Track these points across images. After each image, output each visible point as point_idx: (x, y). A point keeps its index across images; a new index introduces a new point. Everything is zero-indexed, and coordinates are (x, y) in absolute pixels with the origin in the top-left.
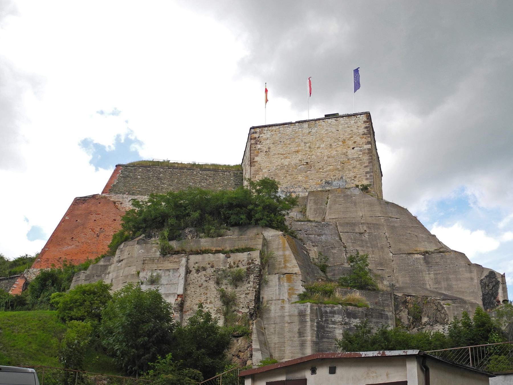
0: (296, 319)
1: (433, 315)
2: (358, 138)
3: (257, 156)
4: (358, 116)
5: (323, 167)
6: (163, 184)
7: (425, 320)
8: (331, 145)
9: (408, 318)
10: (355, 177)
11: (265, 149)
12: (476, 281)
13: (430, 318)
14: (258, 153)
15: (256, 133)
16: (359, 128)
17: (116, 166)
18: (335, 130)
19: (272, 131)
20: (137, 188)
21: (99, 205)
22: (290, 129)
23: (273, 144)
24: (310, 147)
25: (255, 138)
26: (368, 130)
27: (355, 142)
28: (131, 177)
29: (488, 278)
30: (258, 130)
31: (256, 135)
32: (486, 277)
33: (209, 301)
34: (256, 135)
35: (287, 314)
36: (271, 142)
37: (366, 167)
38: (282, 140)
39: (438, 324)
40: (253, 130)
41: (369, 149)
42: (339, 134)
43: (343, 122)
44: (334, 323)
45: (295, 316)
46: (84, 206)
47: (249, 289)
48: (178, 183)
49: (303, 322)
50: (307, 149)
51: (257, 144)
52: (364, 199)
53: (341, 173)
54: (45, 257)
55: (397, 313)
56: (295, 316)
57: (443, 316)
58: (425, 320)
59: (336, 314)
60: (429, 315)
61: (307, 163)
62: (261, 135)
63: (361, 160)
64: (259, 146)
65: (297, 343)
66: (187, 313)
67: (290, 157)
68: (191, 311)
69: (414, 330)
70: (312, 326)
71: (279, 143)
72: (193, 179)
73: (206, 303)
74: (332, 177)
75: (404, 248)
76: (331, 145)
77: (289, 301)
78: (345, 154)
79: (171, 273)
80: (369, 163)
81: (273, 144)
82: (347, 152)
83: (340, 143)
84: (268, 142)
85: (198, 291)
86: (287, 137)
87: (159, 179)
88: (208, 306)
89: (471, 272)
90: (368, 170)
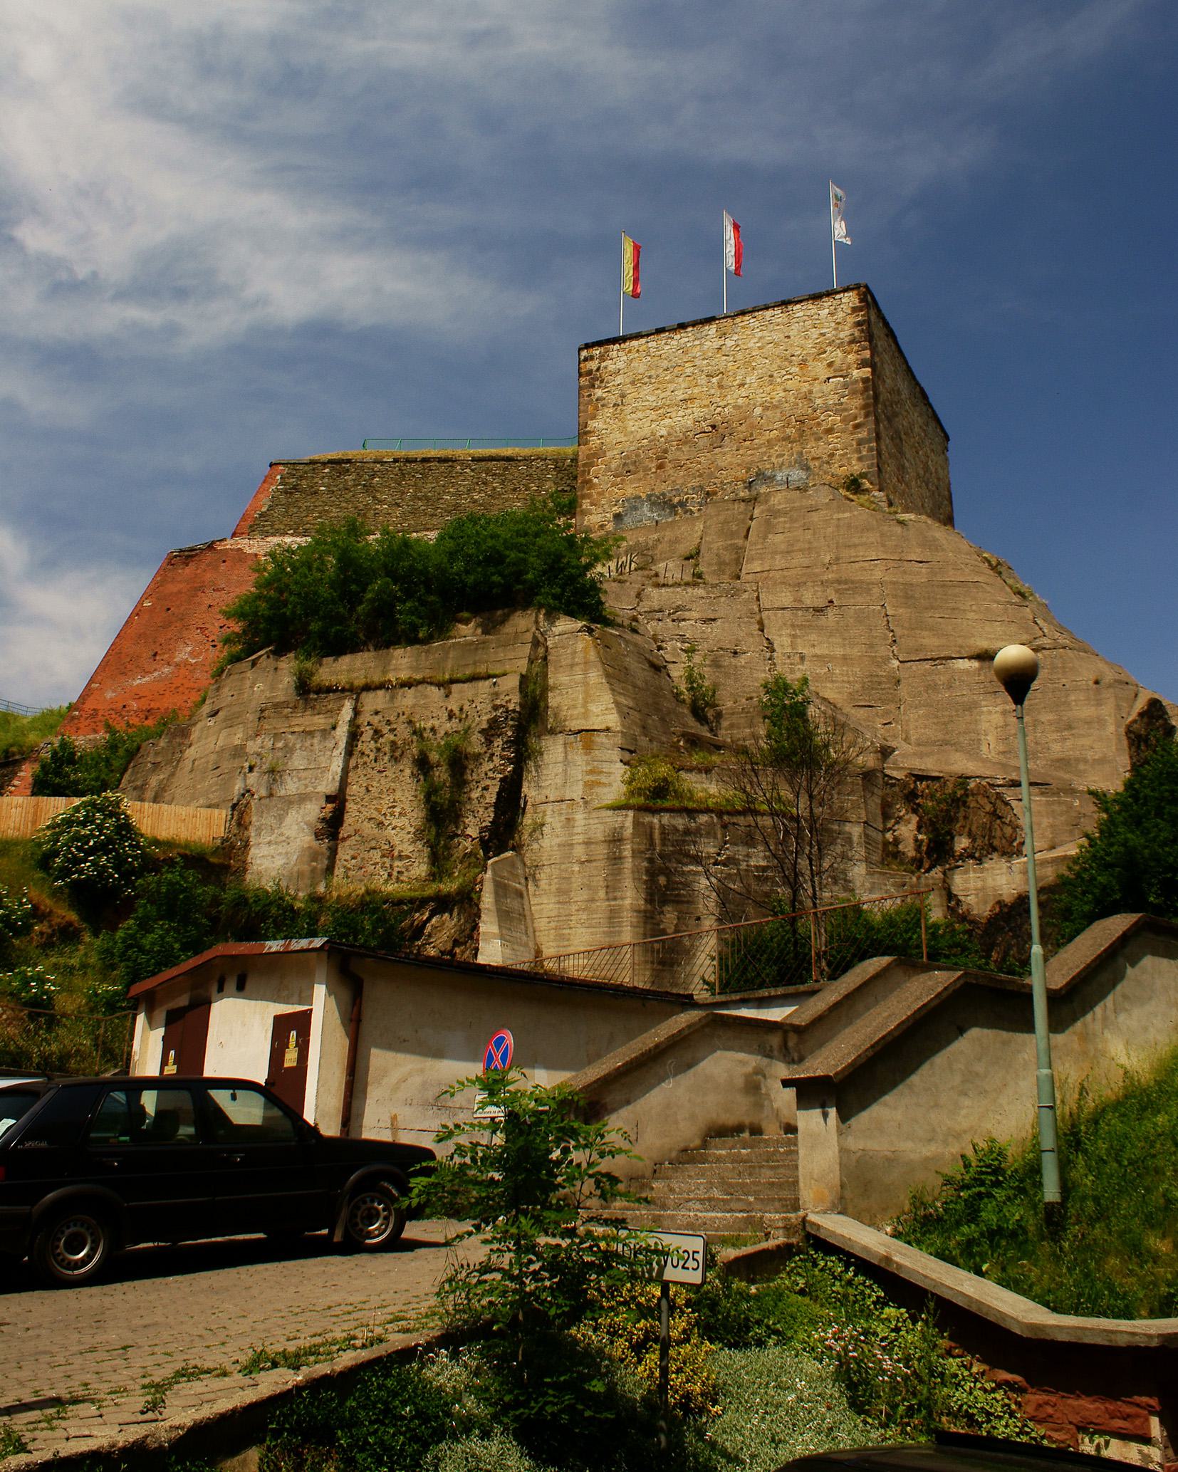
0: (602, 851)
1: (984, 828)
2: (839, 353)
3: (594, 417)
4: (838, 297)
5: (751, 435)
6: (381, 502)
7: (963, 846)
8: (771, 376)
9: (916, 840)
10: (832, 455)
11: (613, 399)
12: (1111, 728)
13: (974, 840)
14: (596, 409)
15: (591, 358)
16: (840, 327)
17: (271, 465)
18: (782, 336)
19: (630, 351)
20: (315, 518)
21: (223, 567)
22: (675, 343)
23: (633, 383)
24: (720, 386)
25: (590, 372)
26: (862, 331)
27: (830, 365)
28: (303, 491)
29: (1145, 720)
30: (596, 352)
31: (593, 365)
32: (1141, 715)
33: (397, 810)
34: (593, 365)
35: (580, 838)
36: (628, 381)
37: (857, 426)
38: (653, 373)
39: (995, 855)
40: (584, 353)
41: (865, 380)
42: (792, 345)
43: (801, 314)
44: (697, 860)
45: (596, 843)
46: (188, 570)
47: (490, 774)
48: (415, 498)
49: (615, 859)
50: (712, 391)
51: (593, 386)
52: (841, 516)
53: (797, 447)
54: (89, 705)
55: (889, 825)
56: (596, 843)
57: (1008, 830)
58: (962, 843)
59: (701, 836)
60: (974, 829)
61: (714, 427)
62: (603, 364)
63: (846, 410)
64: (599, 393)
65: (600, 916)
66: (347, 843)
67: (673, 415)
68: (357, 838)
69: (933, 873)
70: (635, 870)
71: (646, 380)
72: (453, 485)
73: (392, 814)
74: (773, 460)
75: (930, 642)
76: (771, 376)
77: (586, 803)
78: (808, 397)
79: (316, 741)
80: (867, 416)
81: (633, 383)
82: (811, 392)
83: (795, 369)
84: (619, 380)
85: (374, 784)
86: (665, 364)
87: (368, 488)
88: (394, 823)
89: (1099, 703)
90: (863, 434)
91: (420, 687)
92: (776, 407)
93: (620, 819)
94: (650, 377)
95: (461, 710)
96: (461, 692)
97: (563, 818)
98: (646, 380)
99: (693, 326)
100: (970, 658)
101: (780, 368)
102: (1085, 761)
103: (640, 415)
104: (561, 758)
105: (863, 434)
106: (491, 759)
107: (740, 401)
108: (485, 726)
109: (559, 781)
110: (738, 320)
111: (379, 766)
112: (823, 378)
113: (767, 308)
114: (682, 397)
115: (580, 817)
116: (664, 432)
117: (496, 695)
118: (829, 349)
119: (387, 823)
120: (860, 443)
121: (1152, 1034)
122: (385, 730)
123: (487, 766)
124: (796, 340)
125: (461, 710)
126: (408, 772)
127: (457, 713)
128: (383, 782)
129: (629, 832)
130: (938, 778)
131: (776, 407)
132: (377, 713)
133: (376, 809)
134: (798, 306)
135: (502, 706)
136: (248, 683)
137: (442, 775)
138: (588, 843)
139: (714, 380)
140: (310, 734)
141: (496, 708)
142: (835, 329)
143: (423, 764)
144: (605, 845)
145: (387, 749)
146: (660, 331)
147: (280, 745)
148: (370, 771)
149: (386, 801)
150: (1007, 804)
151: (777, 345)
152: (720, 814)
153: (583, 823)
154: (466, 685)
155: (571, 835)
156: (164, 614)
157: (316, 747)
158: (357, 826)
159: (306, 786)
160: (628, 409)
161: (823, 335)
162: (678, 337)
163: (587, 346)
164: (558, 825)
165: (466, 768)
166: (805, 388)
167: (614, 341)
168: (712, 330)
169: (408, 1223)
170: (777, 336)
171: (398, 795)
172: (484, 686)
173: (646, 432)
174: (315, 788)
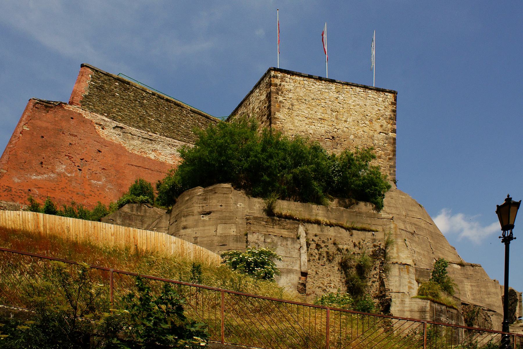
4: (386, 94)
5: (349, 147)
15: (277, 77)
19: (295, 82)
27: (382, 126)
30: (279, 75)
33: (332, 285)
34: (278, 81)
35: (408, 309)
36: (295, 98)
37: (390, 159)
40: (273, 73)
45: (415, 312)
56: (415, 312)
57: (490, 325)
62: (283, 83)
63: (386, 150)
73: (330, 287)
76: (358, 122)
78: (372, 138)
79: (289, 243)
81: (297, 100)
82: (373, 136)
84: (291, 95)
85: (320, 271)
86: (312, 96)
91: (336, 227)
92: (360, 138)
93: (424, 303)
94: (305, 100)
95: (359, 243)
96: (358, 235)
97: (400, 300)
98: (303, 101)
99: (325, 81)
100: (458, 264)
101: (362, 120)
102: (495, 306)
103: (301, 118)
104: (397, 274)
106: (375, 269)
107: (345, 129)
108: (371, 254)
109: (397, 284)
110: (345, 87)
111: (321, 262)
112: (379, 131)
113: (357, 86)
114: (320, 117)
115: (407, 300)
116: (311, 132)
117: (374, 240)
118: (381, 118)
119: (328, 290)
122: (323, 245)
123: (373, 272)
124: (369, 108)
125: (359, 243)
126: (336, 268)
127: (358, 245)
128: (324, 270)
129: (428, 309)
130: (467, 305)
131: (360, 138)
132: (316, 236)
133: (322, 283)
134: (370, 91)
135: (377, 246)
136: (232, 201)
137: (353, 272)
138: (411, 311)
139: (334, 114)
140: (286, 238)
141: (375, 246)
142: (384, 110)
143: (344, 266)
144: (419, 313)
145: (325, 255)
146: (310, 77)
147: (269, 240)
148: (317, 264)
149: (326, 281)
150: (489, 316)
151: (361, 107)
152: (447, 306)
153: (409, 303)
154: (360, 232)
155: (404, 307)
156: (41, 139)
157: (290, 246)
158: (314, 289)
159: (288, 266)
160: (295, 114)
161: (379, 110)
162: (318, 83)
163: (275, 69)
164: (397, 302)
165: (364, 271)
166: (371, 133)
168: (333, 86)
170: (361, 103)
171: (332, 278)
172: (370, 233)
173: (303, 129)
174: (293, 267)
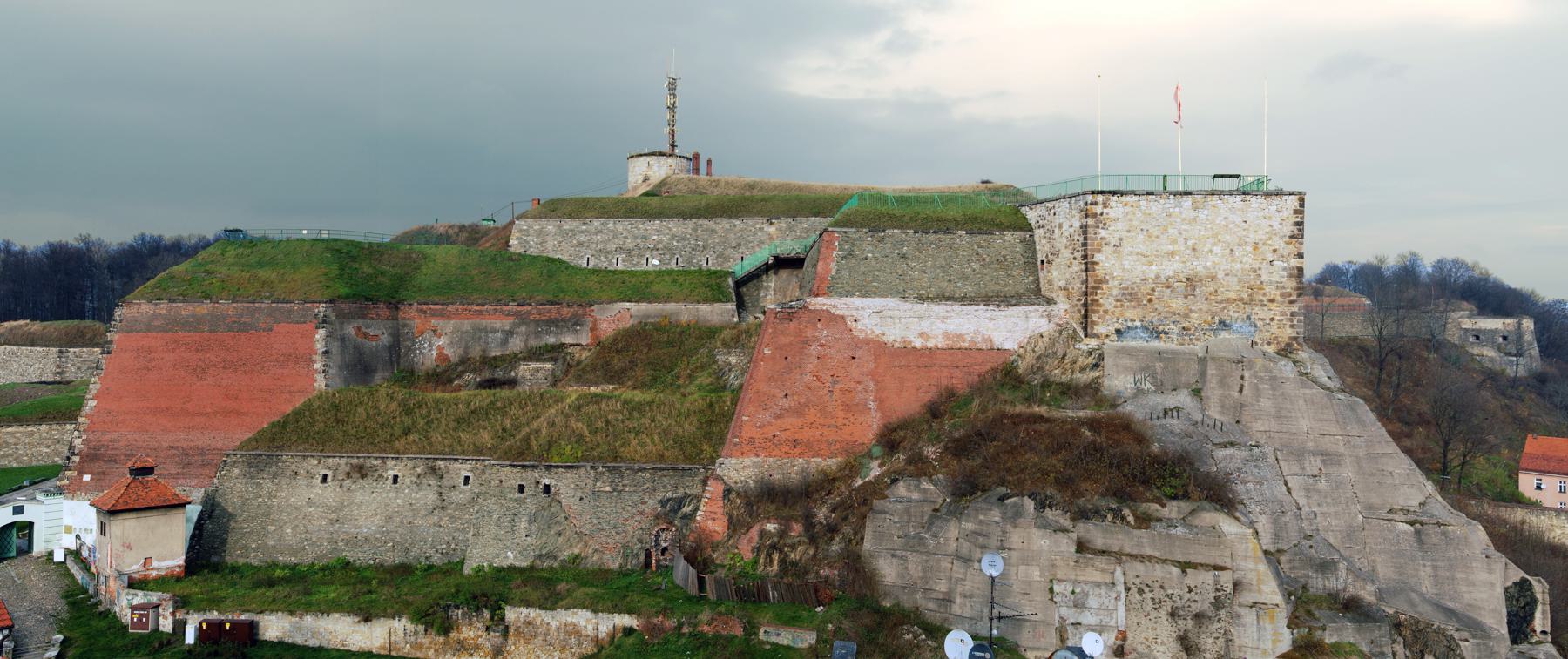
3: (1099, 251)
11: (1113, 241)
15: (1096, 203)
30: (1100, 198)
31: (1098, 209)
34: (1098, 209)
37: (1291, 302)
46: (792, 325)
89: (1490, 571)
105: (1295, 308)
110: (1209, 198)
120: (1293, 314)
121: (1210, 641)
167: (1114, 193)
169: (262, 638)
